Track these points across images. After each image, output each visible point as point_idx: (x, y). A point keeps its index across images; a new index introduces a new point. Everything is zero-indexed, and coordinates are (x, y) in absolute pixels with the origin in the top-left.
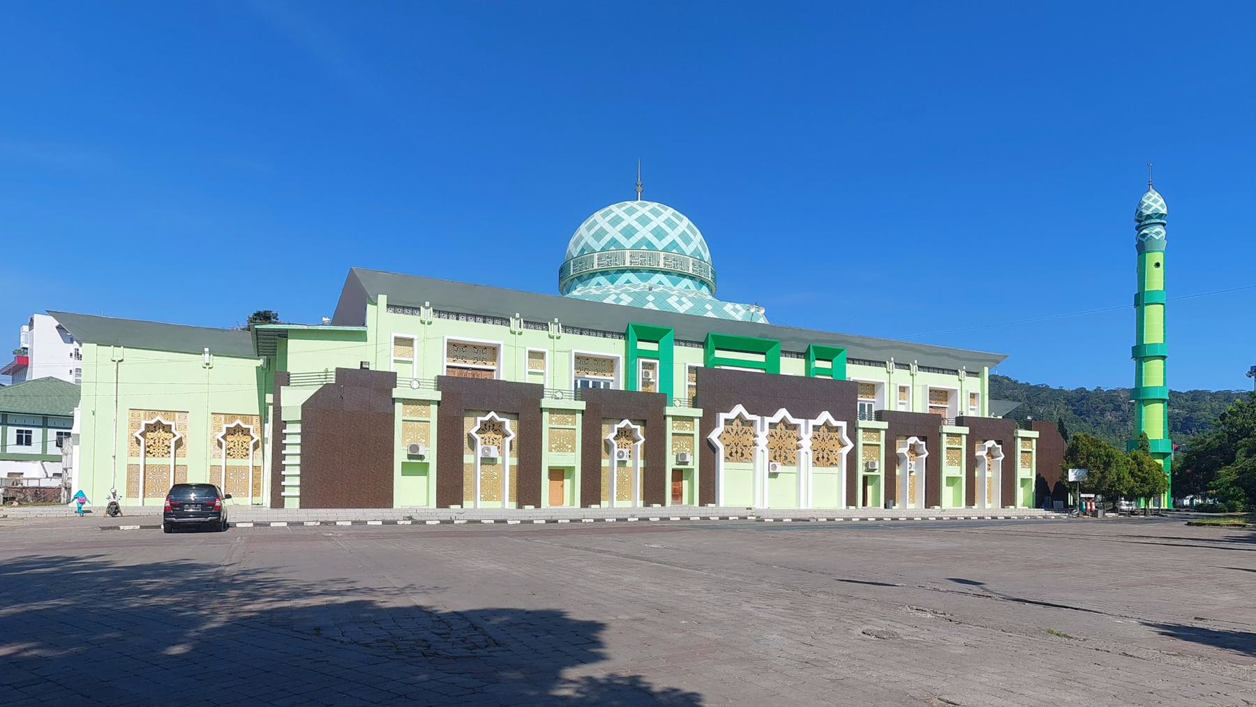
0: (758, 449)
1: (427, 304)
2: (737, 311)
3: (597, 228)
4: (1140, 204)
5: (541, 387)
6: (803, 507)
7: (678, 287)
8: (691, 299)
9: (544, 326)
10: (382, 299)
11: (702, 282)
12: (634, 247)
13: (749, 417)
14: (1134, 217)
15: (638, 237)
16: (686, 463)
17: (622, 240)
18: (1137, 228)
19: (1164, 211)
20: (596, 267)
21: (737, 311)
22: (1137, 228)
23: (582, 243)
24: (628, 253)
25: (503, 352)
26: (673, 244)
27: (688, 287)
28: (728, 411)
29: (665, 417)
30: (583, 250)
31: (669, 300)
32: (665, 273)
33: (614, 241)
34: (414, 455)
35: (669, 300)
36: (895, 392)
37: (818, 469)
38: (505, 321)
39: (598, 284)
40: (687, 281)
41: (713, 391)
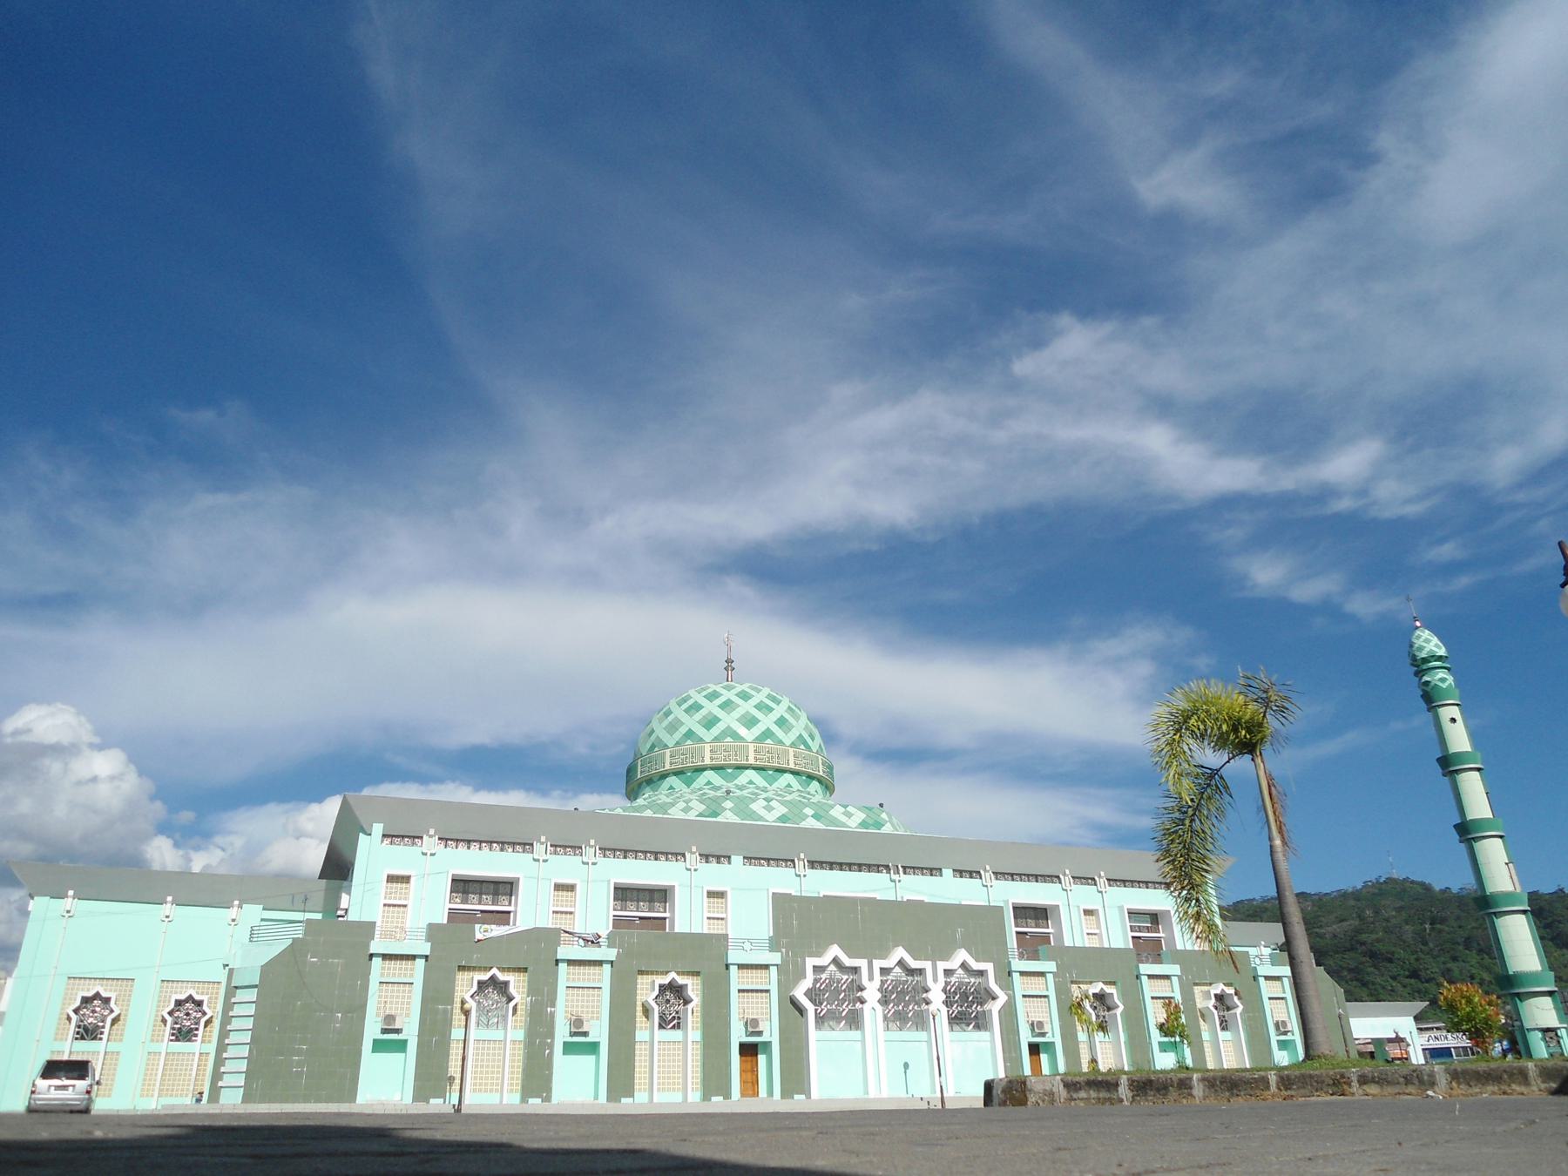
0: (866, 1007)
1: (432, 832)
2: (849, 815)
3: (670, 718)
4: (1411, 646)
5: (725, 937)
6: (873, 1094)
7: (776, 785)
8: (783, 803)
9: (576, 849)
10: (378, 829)
11: (811, 777)
12: (716, 739)
13: (914, 964)
14: (1409, 661)
15: (720, 727)
16: (760, 1033)
17: (700, 731)
18: (1416, 674)
19: (1442, 652)
20: (667, 767)
21: (849, 815)
22: (1416, 674)
23: (653, 737)
24: (707, 748)
25: (523, 889)
26: (768, 734)
27: (789, 786)
28: (819, 955)
29: (727, 967)
30: (653, 746)
31: (753, 806)
32: (795, 773)
33: (690, 734)
34: (578, 1028)
35: (753, 806)
36: (1077, 916)
37: (896, 1035)
38: (527, 846)
39: (671, 788)
40: (788, 777)
41: (798, 923)
